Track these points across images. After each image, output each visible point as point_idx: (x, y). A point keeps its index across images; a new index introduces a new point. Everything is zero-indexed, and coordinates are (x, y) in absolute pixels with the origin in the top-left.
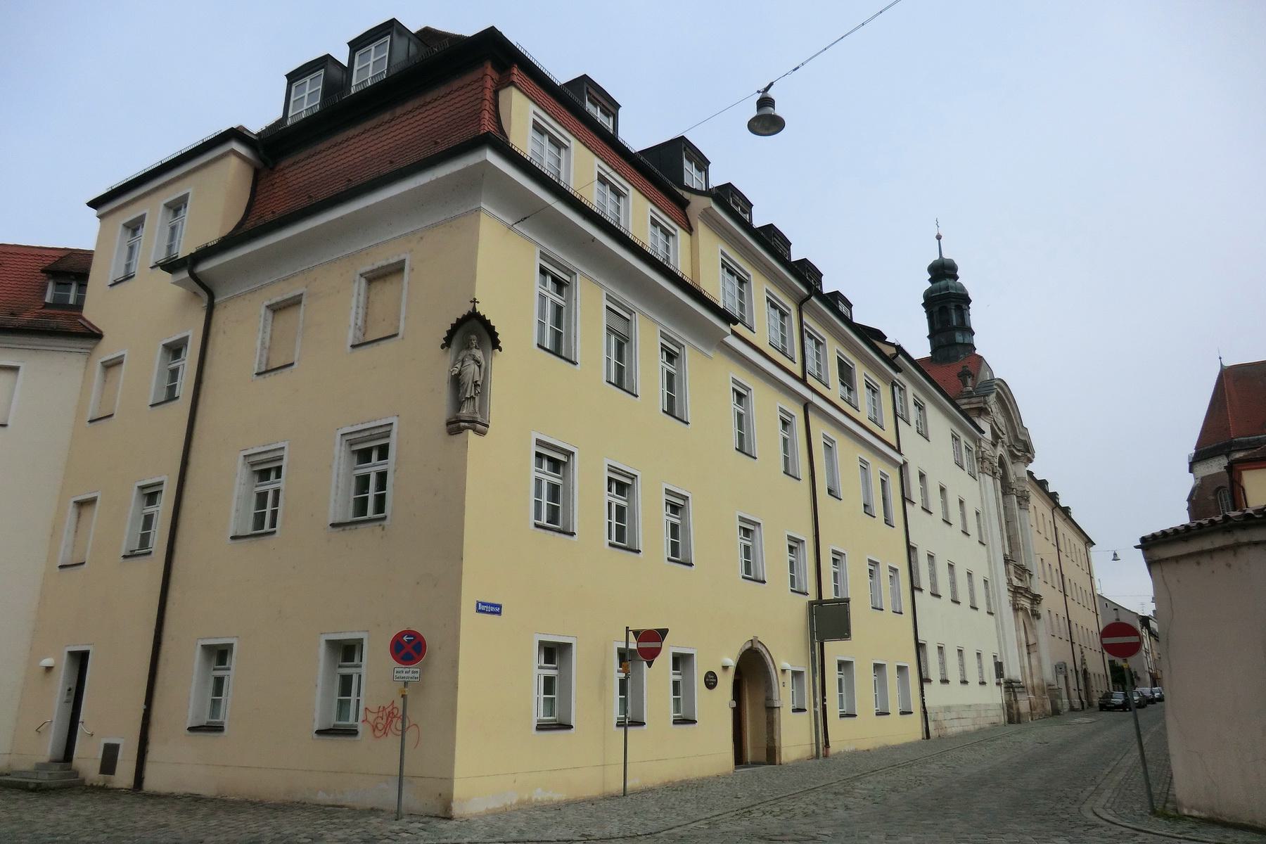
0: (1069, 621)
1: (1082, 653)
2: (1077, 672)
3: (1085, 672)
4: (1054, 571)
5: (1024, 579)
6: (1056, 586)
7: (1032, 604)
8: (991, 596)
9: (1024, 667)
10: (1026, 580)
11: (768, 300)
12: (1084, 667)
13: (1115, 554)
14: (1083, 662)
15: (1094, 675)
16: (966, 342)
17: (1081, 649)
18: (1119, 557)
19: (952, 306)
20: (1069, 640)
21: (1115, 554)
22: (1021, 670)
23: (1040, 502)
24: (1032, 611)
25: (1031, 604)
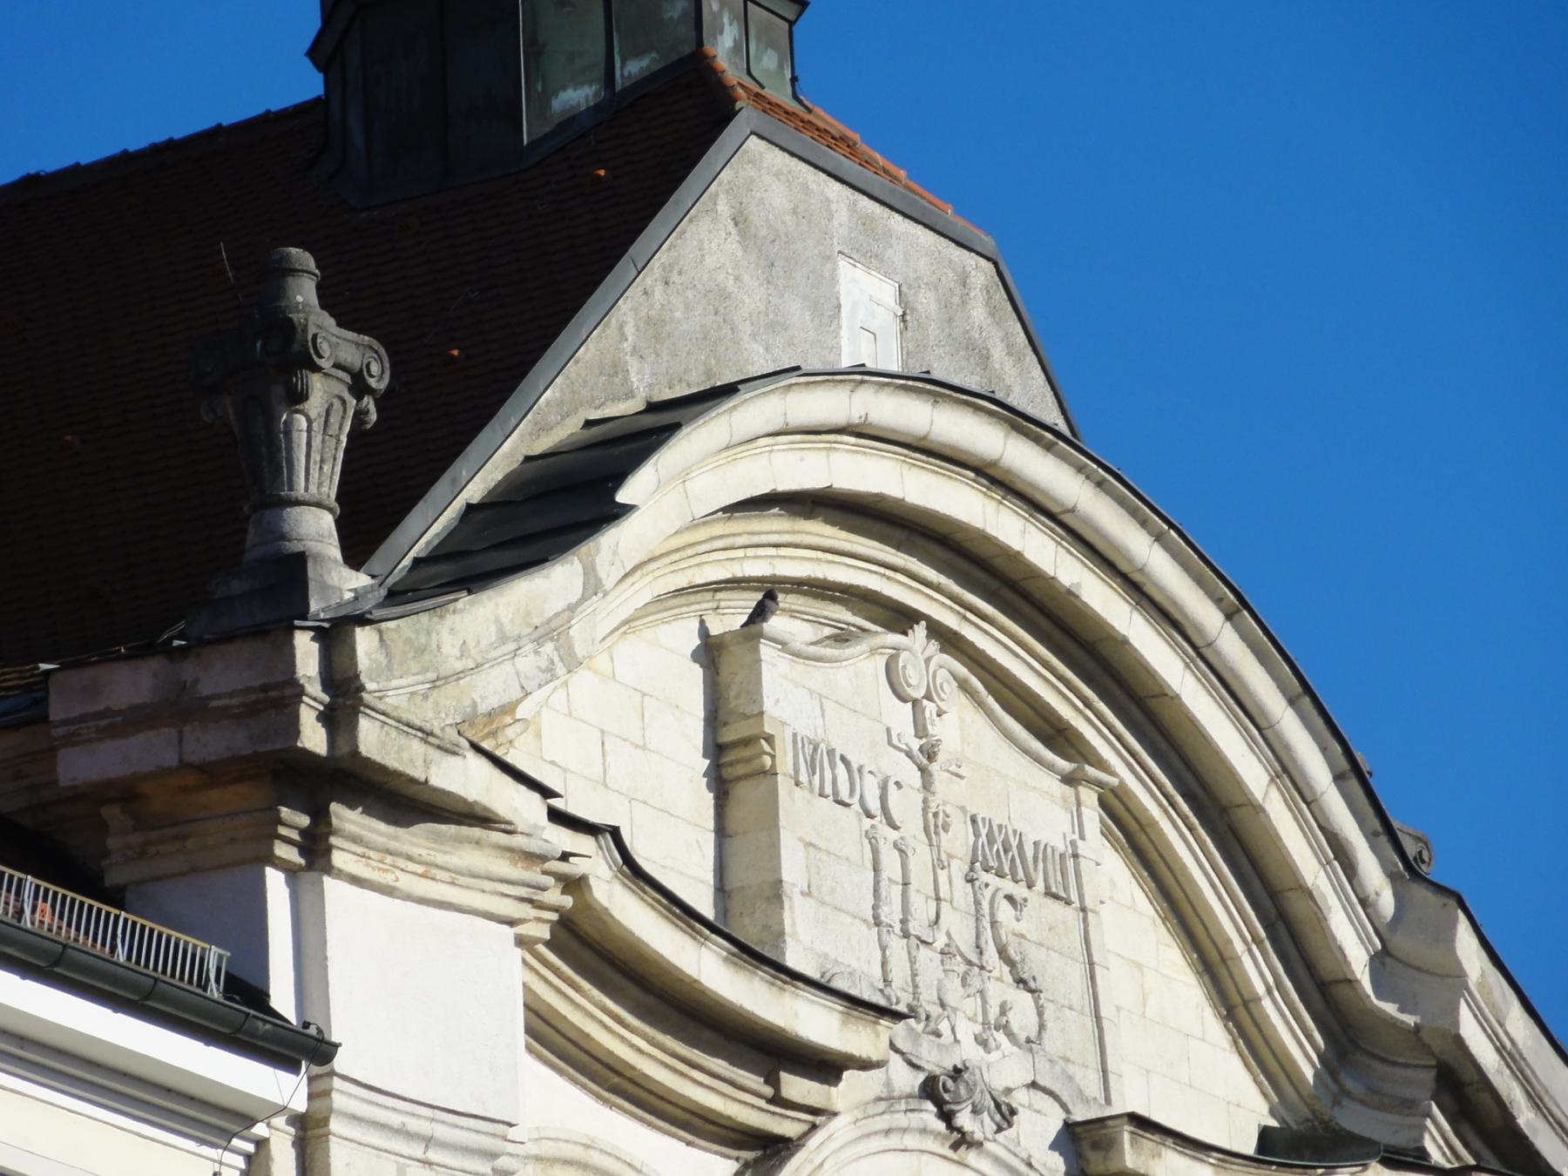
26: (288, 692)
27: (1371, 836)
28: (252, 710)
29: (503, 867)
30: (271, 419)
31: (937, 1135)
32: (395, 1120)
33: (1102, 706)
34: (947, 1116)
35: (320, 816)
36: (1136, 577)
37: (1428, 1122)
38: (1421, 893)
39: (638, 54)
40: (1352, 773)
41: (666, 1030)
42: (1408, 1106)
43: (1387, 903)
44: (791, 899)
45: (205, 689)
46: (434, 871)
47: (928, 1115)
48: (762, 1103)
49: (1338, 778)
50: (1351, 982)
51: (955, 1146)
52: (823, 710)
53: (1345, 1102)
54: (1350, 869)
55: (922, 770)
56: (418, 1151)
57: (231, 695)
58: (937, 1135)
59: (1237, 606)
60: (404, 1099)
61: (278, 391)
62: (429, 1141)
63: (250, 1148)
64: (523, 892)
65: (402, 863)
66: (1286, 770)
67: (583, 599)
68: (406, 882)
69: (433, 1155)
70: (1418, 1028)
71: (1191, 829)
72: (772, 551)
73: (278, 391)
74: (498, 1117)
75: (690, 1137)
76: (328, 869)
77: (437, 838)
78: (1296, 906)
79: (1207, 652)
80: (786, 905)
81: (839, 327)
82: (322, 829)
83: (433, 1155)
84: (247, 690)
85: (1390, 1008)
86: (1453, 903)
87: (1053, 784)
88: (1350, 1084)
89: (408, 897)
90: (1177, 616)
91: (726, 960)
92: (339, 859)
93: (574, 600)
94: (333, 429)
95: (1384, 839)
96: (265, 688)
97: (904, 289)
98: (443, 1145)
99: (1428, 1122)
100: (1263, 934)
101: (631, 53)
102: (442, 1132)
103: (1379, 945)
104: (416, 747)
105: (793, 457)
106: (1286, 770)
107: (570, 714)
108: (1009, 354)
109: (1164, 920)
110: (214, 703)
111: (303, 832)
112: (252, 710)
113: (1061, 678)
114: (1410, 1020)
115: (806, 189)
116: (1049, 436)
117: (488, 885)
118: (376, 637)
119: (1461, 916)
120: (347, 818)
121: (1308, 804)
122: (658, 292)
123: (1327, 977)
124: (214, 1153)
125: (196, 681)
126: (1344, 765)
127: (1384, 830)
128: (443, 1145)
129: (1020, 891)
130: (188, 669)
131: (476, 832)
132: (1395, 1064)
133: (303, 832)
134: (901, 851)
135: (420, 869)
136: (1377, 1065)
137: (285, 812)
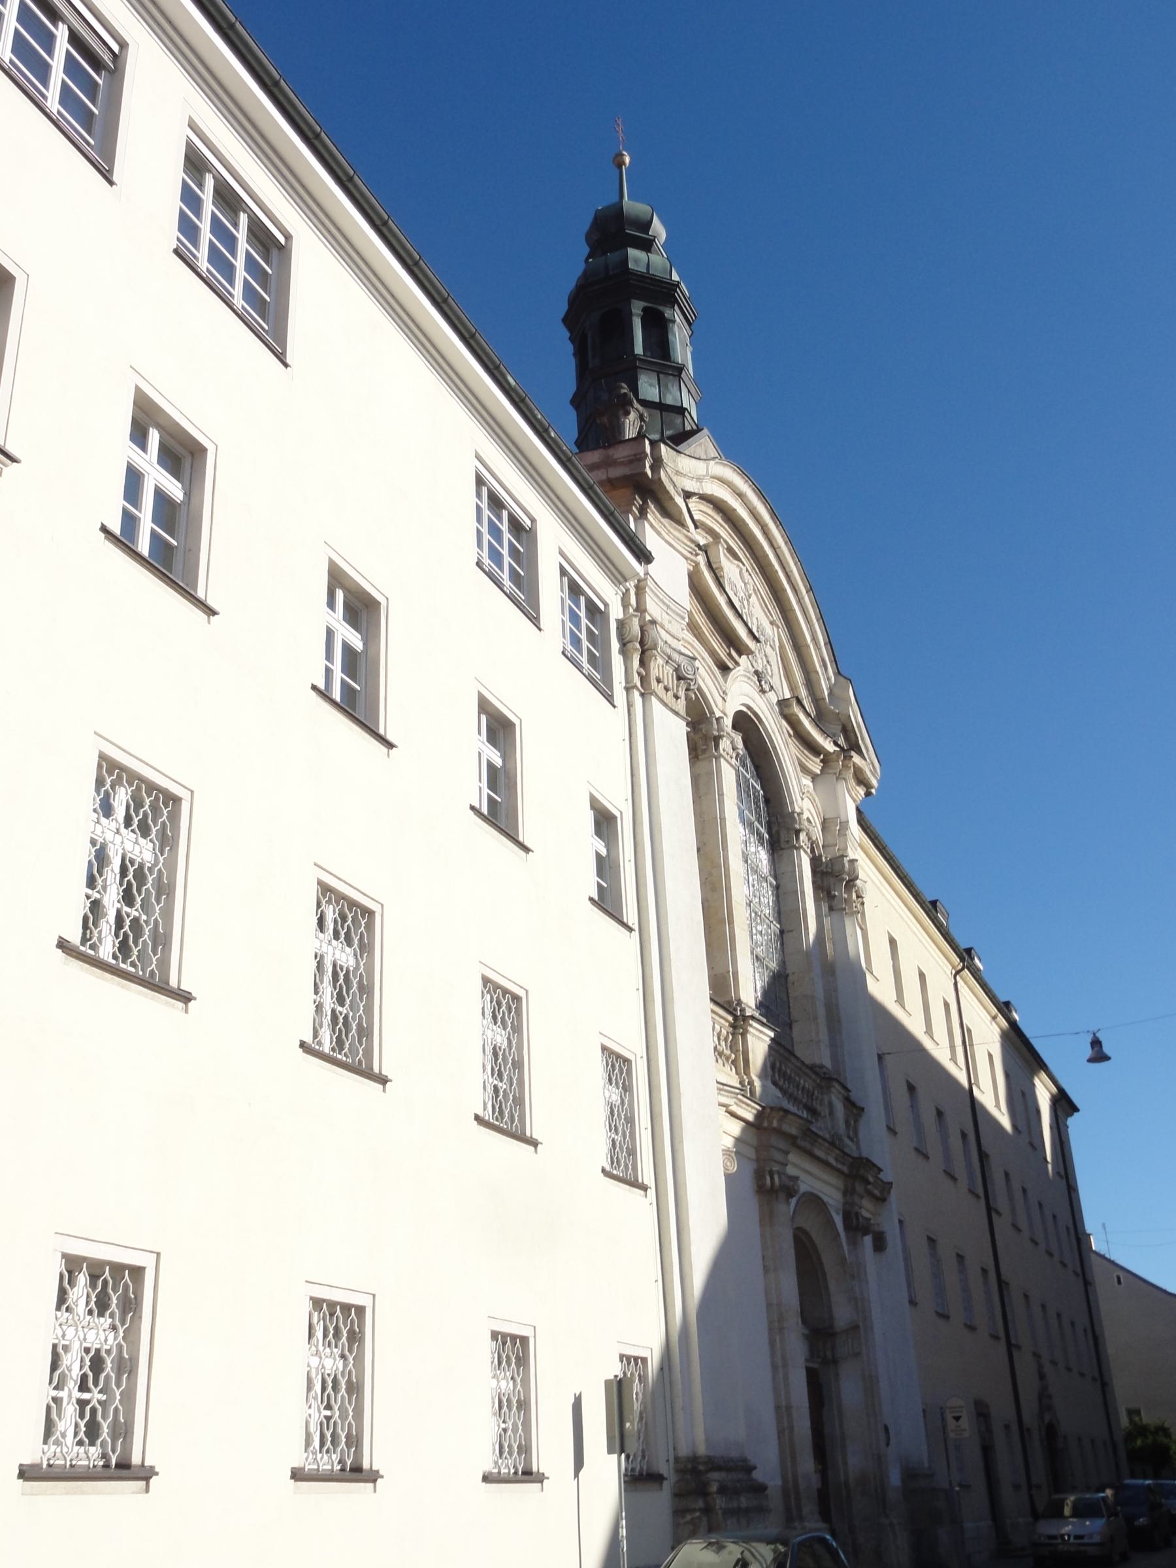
0: (1002, 1284)
1: (1042, 1376)
2: (1023, 1431)
3: (1051, 1431)
4: (955, 1142)
5: (825, 1111)
6: (960, 1171)
7: (847, 1192)
8: (893, 864)
9: (789, 1408)
10: (831, 1113)
11: (563, 572)
12: (1047, 1418)
13: (1096, 1043)
14: (1044, 1396)
15: (1080, 1439)
16: (669, 400)
17: (1040, 1367)
18: (1107, 1049)
19: (637, 307)
20: (1002, 1334)
21: (1096, 1043)
22: (779, 1419)
23: (906, 870)
24: (847, 1216)
25: (845, 1193)
26: (643, 455)
27: (831, 662)
28: (631, 462)
30: (618, 419)
33: (777, 609)
34: (760, 681)
35: (645, 502)
36: (789, 574)
38: (842, 679)
39: (669, 430)
40: (829, 643)
41: (710, 621)
45: (615, 457)
46: (670, 534)
47: (755, 679)
48: (726, 654)
49: (825, 644)
50: (824, 699)
51: (760, 691)
54: (826, 669)
57: (624, 457)
59: (810, 589)
60: (663, 591)
61: (621, 412)
64: (690, 550)
66: (814, 639)
69: (668, 611)
70: (839, 713)
73: (621, 412)
74: (316, 1282)
78: (813, 676)
79: (802, 601)
82: (646, 506)
84: (629, 456)
86: (849, 682)
89: (663, 538)
90: (797, 588)
94: (635, 426)
95: (834, 663)
96: (635, 455)
101: (669, 429)
106: (814, 639)
110: (619, 460)
112: (631, 462)
113: (770, 598)
116: (778, 523)
117: (682, 545)
123: (818, 698)
125: (613, 454)
127: (835, 661)
130: (611, 452)
131: (680, 528)
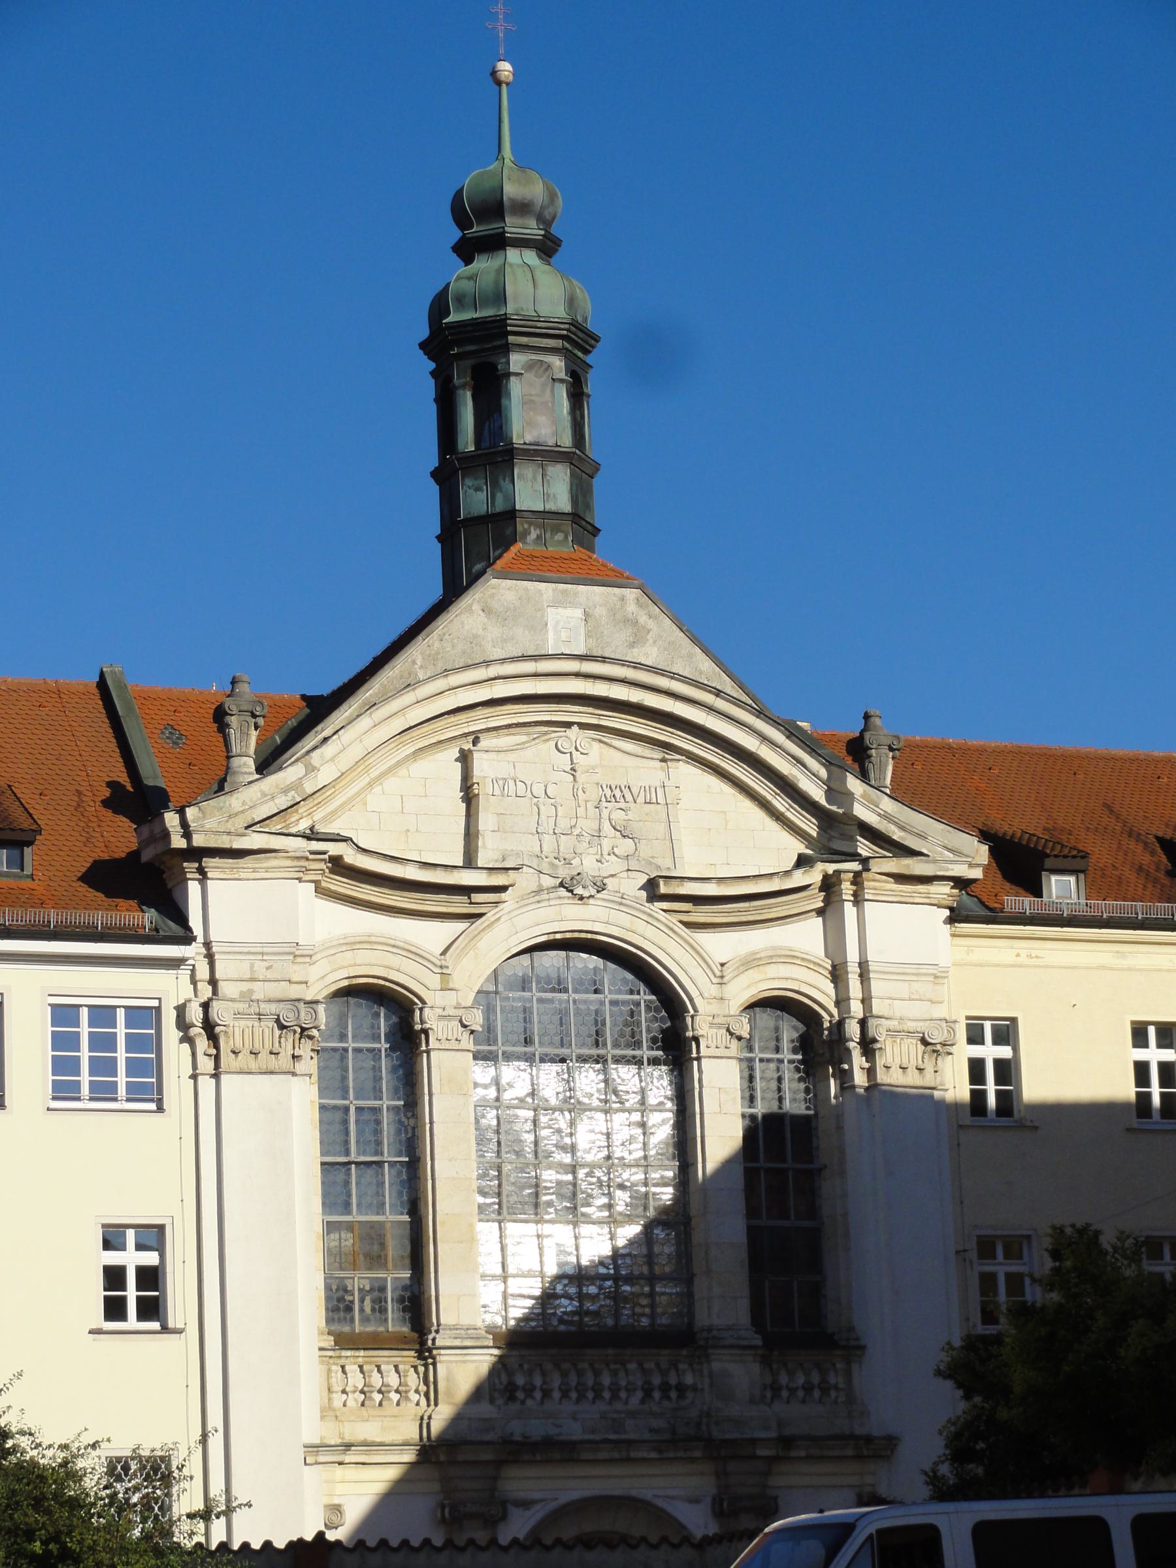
29: (289, 863)
31: (569, 898)
32: (246, 950)
37: (858, 843)
42: (852, 839)
43: (823, 773)
44: (483, 835)
47: (563, 892)
48: (467, 905)
49: (788, 737)
52: (514, 766)
53: (834, 840)
55: (573, 775)
56: (260, 957)
58: (569, 898)
62: (263, 954)
63: (191, 967)
64: (297, 869)
65: (242, 870)
66: (764, 738)
67: (306, 775)
68: (243, 875)
69: (265, 958)
71: (736, 763)
72: (485, 720)
75: (441, 920)
76: (208, 879)
77: (257, 859)
80: (480, 838)
81: (547, 631)
83: (265, 958)
85: (834, 808)
87: (658, 764)
88: (833, 833)
91: (419, 868)
92: (209, 875)
93: (301, 776)
97: (587, 610)
98: (267, 954)
99: (858, 843)
100: (778, 792)
102: (265, 950)
103: (826, 788)
104: (226, 838)
105: (504, 686)
106: (764, 738)
107: (383, 793)
108: (650, 617)
109: (740, 793)
111: (197, 869)
114: (841, 811)
115: (527, 589)
118: (197, 809)
119: (848, 774)
120: (207, 862)
121: (779, 747)
122: (437, 645)
124: (175, 972)
126: (788, 733)
128: (267, 954)
129: (622, 805)
132: (848, 824)
133: (197, 869)
134: (555, 806)
135: (251, 870)
136: (842, 825)
137: (185, 864)
